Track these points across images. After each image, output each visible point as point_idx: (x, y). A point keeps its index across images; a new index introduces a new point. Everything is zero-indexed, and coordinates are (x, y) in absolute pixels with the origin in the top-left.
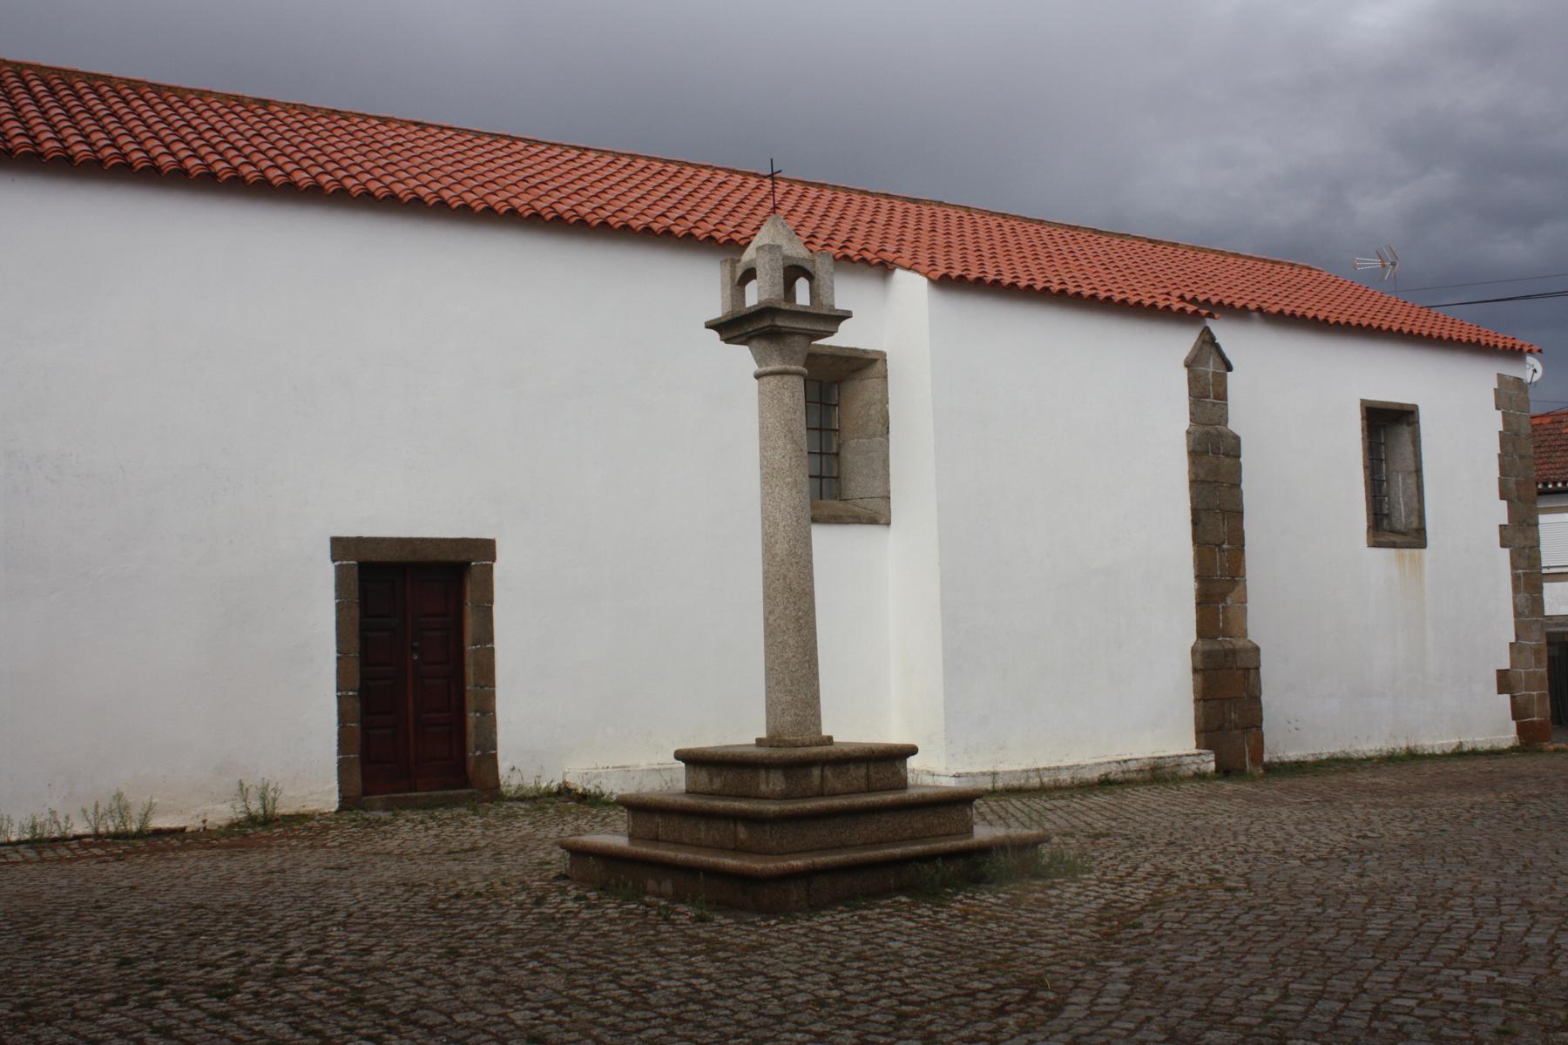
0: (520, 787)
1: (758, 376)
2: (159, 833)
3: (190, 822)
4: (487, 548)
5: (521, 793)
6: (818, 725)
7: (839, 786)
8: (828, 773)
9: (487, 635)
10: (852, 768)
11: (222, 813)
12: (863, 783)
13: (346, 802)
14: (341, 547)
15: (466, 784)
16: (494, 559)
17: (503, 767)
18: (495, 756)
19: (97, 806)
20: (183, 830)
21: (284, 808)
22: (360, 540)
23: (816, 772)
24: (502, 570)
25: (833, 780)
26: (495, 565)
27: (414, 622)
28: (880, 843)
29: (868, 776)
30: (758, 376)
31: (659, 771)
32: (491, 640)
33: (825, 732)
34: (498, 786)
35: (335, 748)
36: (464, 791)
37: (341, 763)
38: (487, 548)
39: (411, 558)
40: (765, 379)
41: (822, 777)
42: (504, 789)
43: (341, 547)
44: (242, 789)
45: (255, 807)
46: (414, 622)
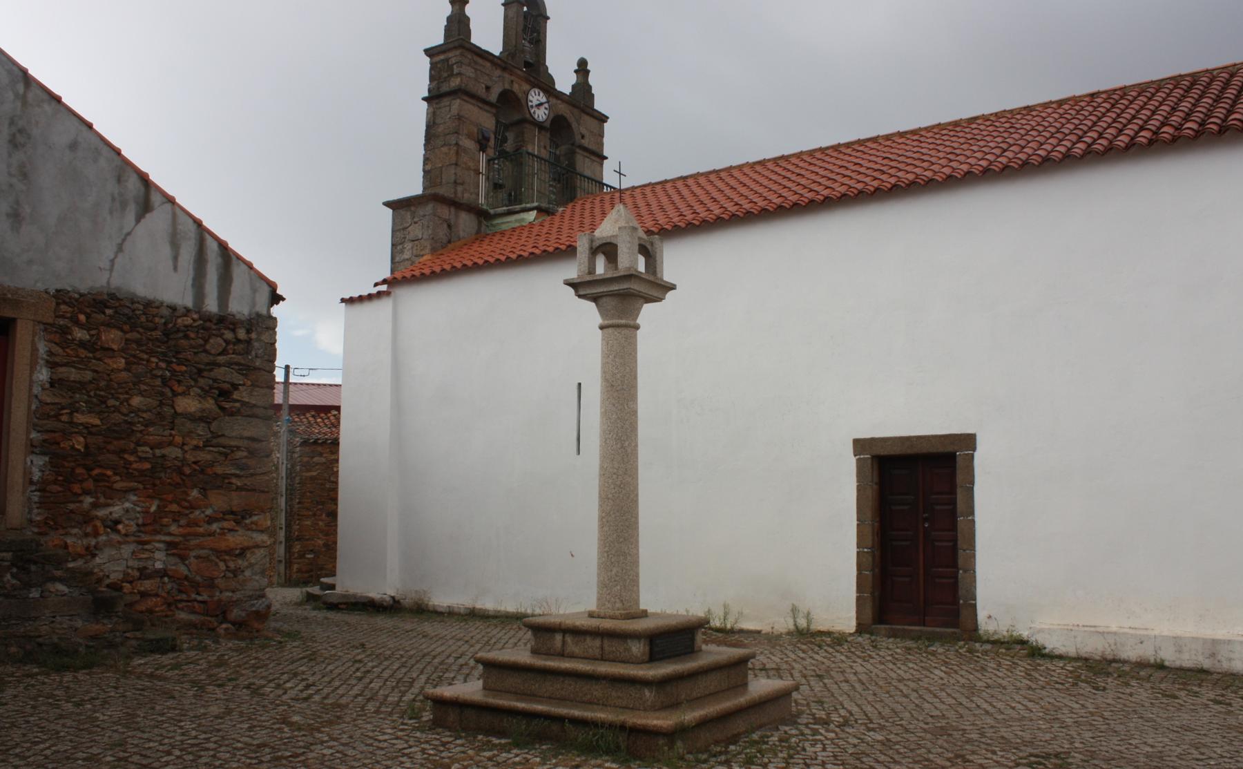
0: (995, 632)
1: (602, 328)
2: (741, 631)
3: (763, 627)
4: (969, 441)
5: (996, 637)
6: (637, 602)
7: (577, 650)
8: (569, 639)
9: (971, 511)
10: (588, 639)
11: (783, 624)
12: (597, 652)
13: (861, 629)
14: (860, 445)
15: (955, 625)
16: (974, 449)
17: (981, 615)
18: (975, 606)
19: (726, 614)
20: (759, 632)
21: (816, 626)
22: (873, 439)
23: (558, 638)
24: (981, 458)
25: (572, 645)
26: (976, 454)
27: (915, 502)
28: (562, 700)
29: (602, 648)
30: (602, 328)
31: (1103, 633)
32: (972, 513)
33: (642, 607)
34: (976, 629)
35: (855, 588)
36: (950, 630)
37: (858, 599)
38: (969, 441)
39: (909, 452)
40: (610, 330)
41: (564, 642)
42: (981, 632)
43: (860, 445)
44: (794, 611)
45: (802, 623)
46: (915, 502)
